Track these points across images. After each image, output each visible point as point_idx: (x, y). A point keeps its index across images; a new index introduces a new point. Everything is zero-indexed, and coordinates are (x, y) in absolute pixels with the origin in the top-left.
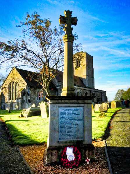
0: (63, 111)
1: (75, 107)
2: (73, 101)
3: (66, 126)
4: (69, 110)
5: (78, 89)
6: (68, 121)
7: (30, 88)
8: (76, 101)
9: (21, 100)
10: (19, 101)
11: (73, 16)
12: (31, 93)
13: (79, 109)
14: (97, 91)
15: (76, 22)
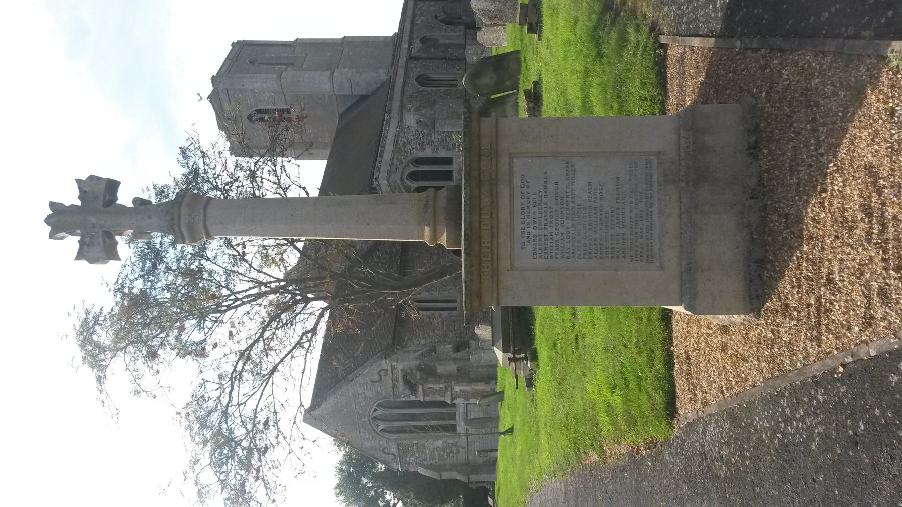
0: (529, 248)
1: (512, 196)
2: (486, 201)
3: (596, 232)
4: (527, 221)
5: (401, 120)
6: (573, 226)
7: (403, 347)
8: (485, 190)
9: (457, 383)
10: (461, 390)
11: (71, 198)
12: (423, 342)
13: (523, 176)
14: (408, 25)
15: (102, 187)
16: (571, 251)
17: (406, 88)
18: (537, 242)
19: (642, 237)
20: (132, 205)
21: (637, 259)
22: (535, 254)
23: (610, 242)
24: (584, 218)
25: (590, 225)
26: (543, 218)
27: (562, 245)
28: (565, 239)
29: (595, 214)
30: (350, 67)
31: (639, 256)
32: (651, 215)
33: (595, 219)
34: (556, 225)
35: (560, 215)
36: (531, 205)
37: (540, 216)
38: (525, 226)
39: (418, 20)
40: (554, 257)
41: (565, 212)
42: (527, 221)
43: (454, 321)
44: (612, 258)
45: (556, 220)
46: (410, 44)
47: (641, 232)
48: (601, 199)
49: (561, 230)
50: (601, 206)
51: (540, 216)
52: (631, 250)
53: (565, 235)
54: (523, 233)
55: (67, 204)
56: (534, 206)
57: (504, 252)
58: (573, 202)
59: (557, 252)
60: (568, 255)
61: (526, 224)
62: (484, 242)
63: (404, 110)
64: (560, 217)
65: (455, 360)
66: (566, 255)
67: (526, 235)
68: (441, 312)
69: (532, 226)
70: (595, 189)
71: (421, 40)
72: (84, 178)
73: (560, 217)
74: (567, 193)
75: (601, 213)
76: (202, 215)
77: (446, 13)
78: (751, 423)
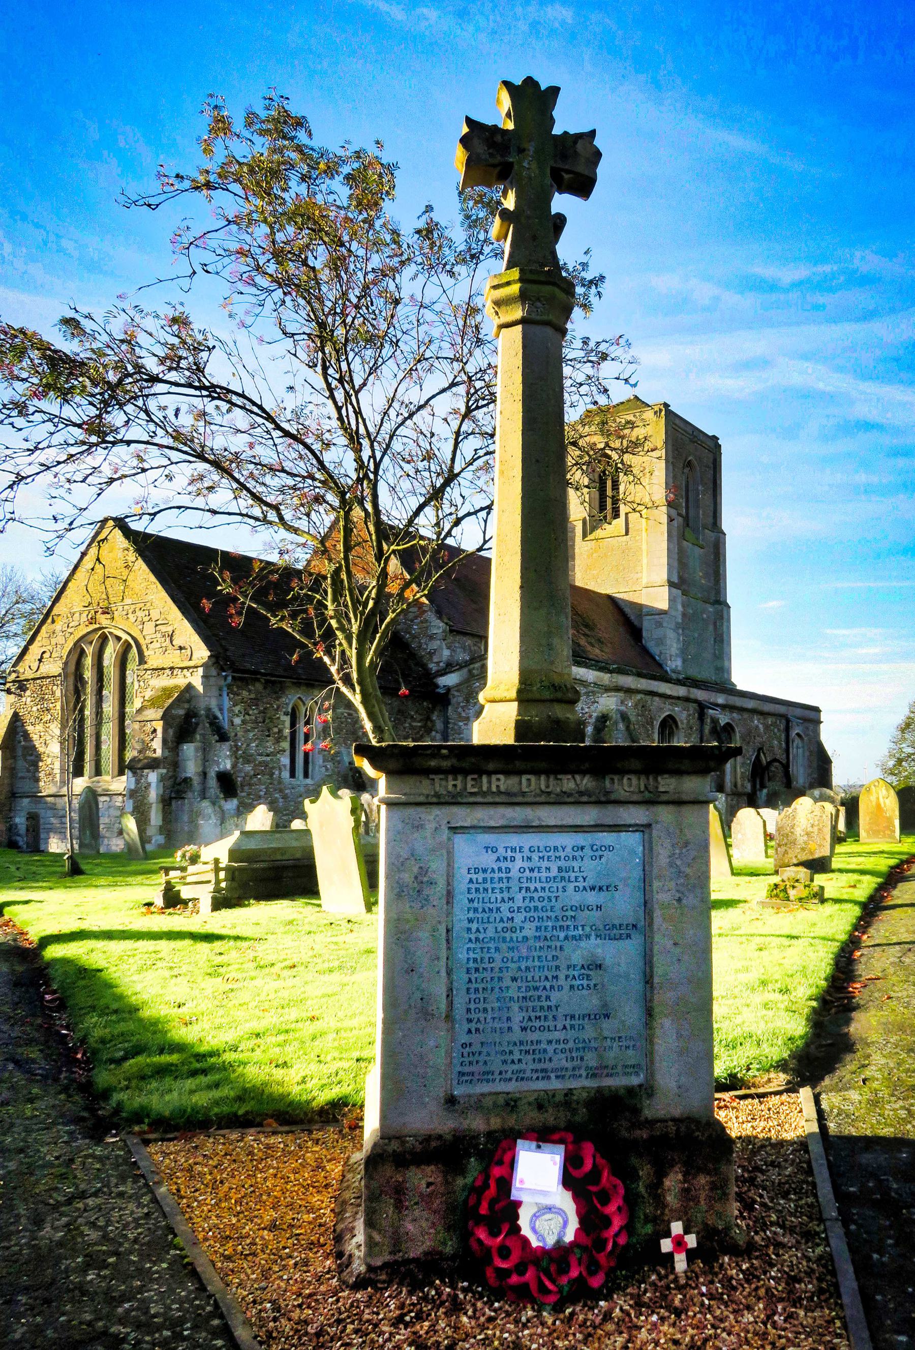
0: (488, 860)
2: (568, 783)
3: (514, 979)
4: (535, 857)
5: (607, 689)
6: (526, 939)
7: (229, 686)
8: (586, 782)
9: (162, 779)
10: (149, 785)
12: (237, 721)
13: (610, 848)
14: (751, 704)
15: (581, 169)
16: (481, 936)
17: (657, 699)
18: (496, 875)
19: (505, 1062)
20: (553, 212)
21: (465, 1054)
22: (477, 871)
23: (497, 1005)
24: (539, 957)
25: (527, 968)
26: (538, 885)
27: (492, 920)
28: (501, 925)
29: (547, 978)
30: (684, 615)
31: (471, 1059)
32: (543, 1078)
33: (537, 978)
34: (527, 909)
35: (544, 914)
36: (562, 863)
37: (544, 879)
38: (526, 853)
39: (759, 720)
40: (471, 905)
41: (550, 924)
42: (535, 857)
43: (272, 774)
44: (469, 1010)
45: (536, 908)
46: (724, 707)
47: (513, 1062)
48: (572, 987)
49: (519, 918)
50: (560, 988)
51: (544, 879)
52: (482, 1043)
53: (509, 925)
54: (513, 850)
55: (557, 113)
56: (560, 869)
57: (480, 815)
58: (566, 938)
59: (480, 910)
60: (474, 930)
61: (529, 855)
62: (498, 780)
63: (621, 694)
64: (541, 914)
65: (204, 774)
66: (474, 926)
67: (509, 854)
68: (288, 753)
69: (526, 865)
70: (588, 976)
71: (728, 724)
72: (596, 142)
73: (541, 914)
74: (583, 926)
75: (548, 987)
76: (538, 318)
77: (769, 764)
78: (152, 1280)
